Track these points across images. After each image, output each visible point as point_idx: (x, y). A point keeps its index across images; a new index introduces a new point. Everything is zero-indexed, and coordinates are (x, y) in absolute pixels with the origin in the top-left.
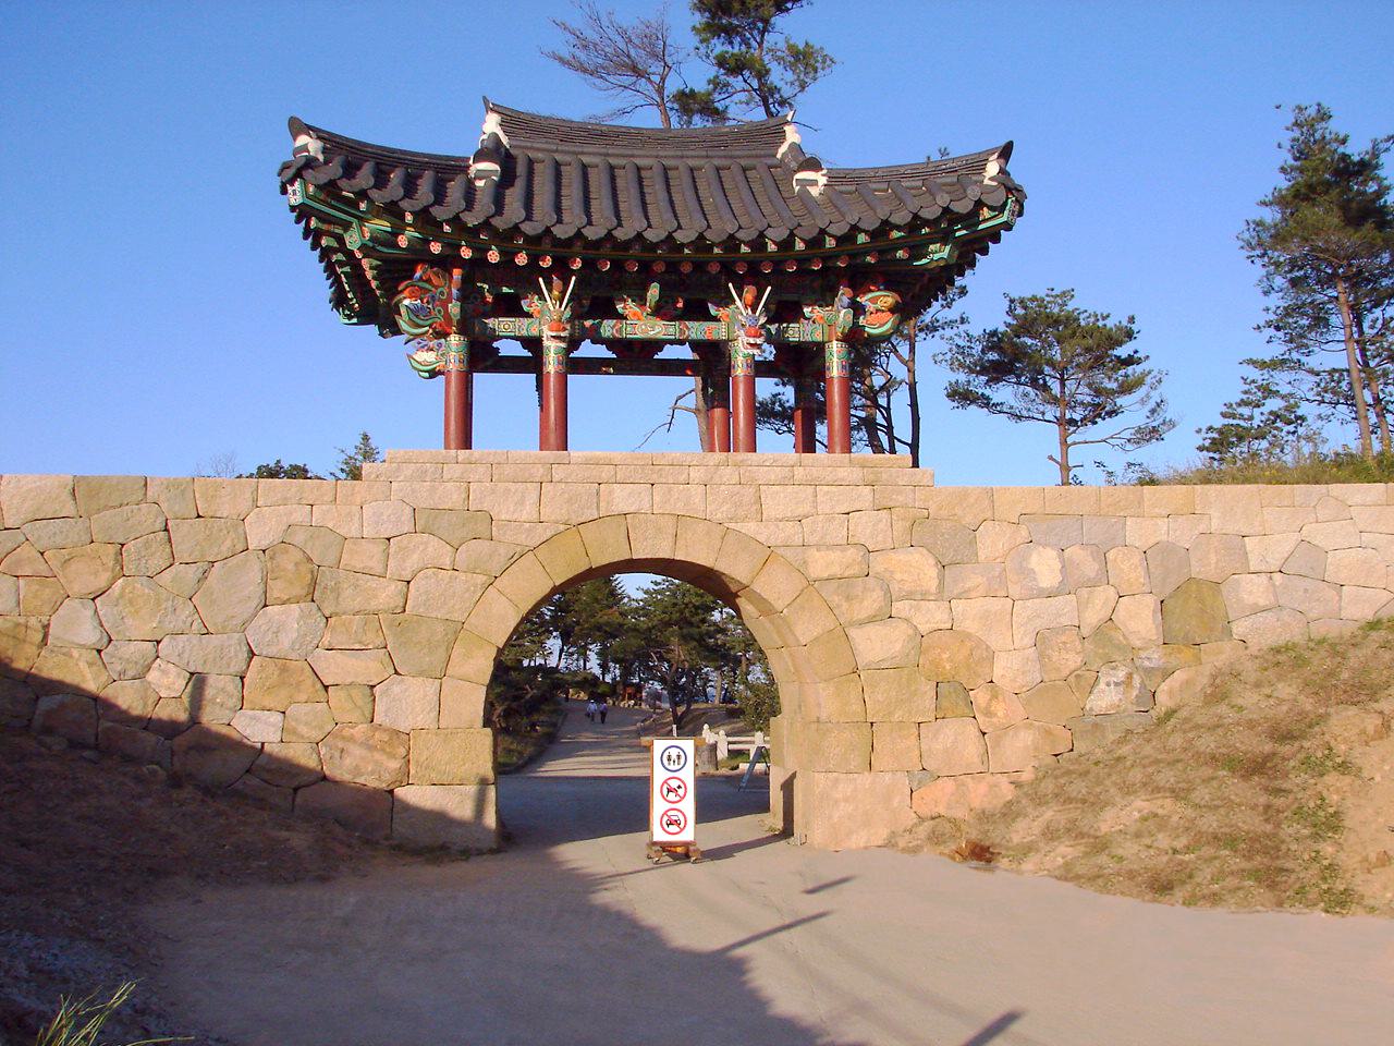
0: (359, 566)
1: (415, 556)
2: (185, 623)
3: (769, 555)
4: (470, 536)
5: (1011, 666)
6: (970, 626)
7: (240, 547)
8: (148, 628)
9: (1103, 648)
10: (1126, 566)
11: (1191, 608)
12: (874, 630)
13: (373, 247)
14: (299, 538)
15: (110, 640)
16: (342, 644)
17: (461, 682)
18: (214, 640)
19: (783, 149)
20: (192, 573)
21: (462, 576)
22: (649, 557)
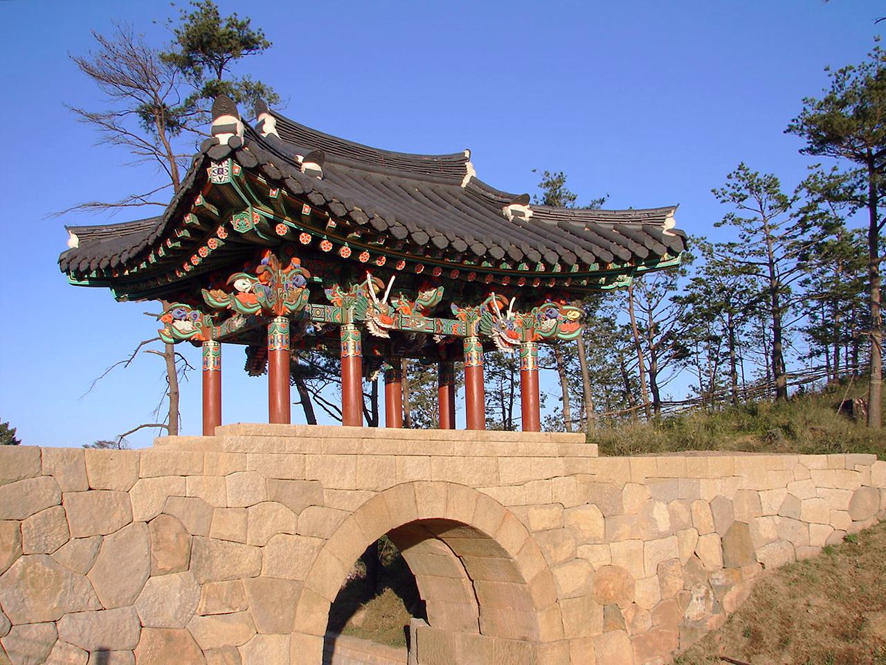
0: (226, 535)
1: (269, 523)
2: (83, 600)
3: (506, 513)
4: (308, 504)
5: (646, 593)
6: (622, 562)
7: (127, 519)
8: (47, 611)
9: (693, 573)
10: (704, 516)
11: (736, 540)
12: (568, 569)
13: (256, 232)
14: (177, 508)
15: (12, 626)
16: (215, 610)
17: (306, 636)
18: (110, 616)
19: (466, 181)
20: (87, 547)
21: (304, 540)
22: (430, 517)
